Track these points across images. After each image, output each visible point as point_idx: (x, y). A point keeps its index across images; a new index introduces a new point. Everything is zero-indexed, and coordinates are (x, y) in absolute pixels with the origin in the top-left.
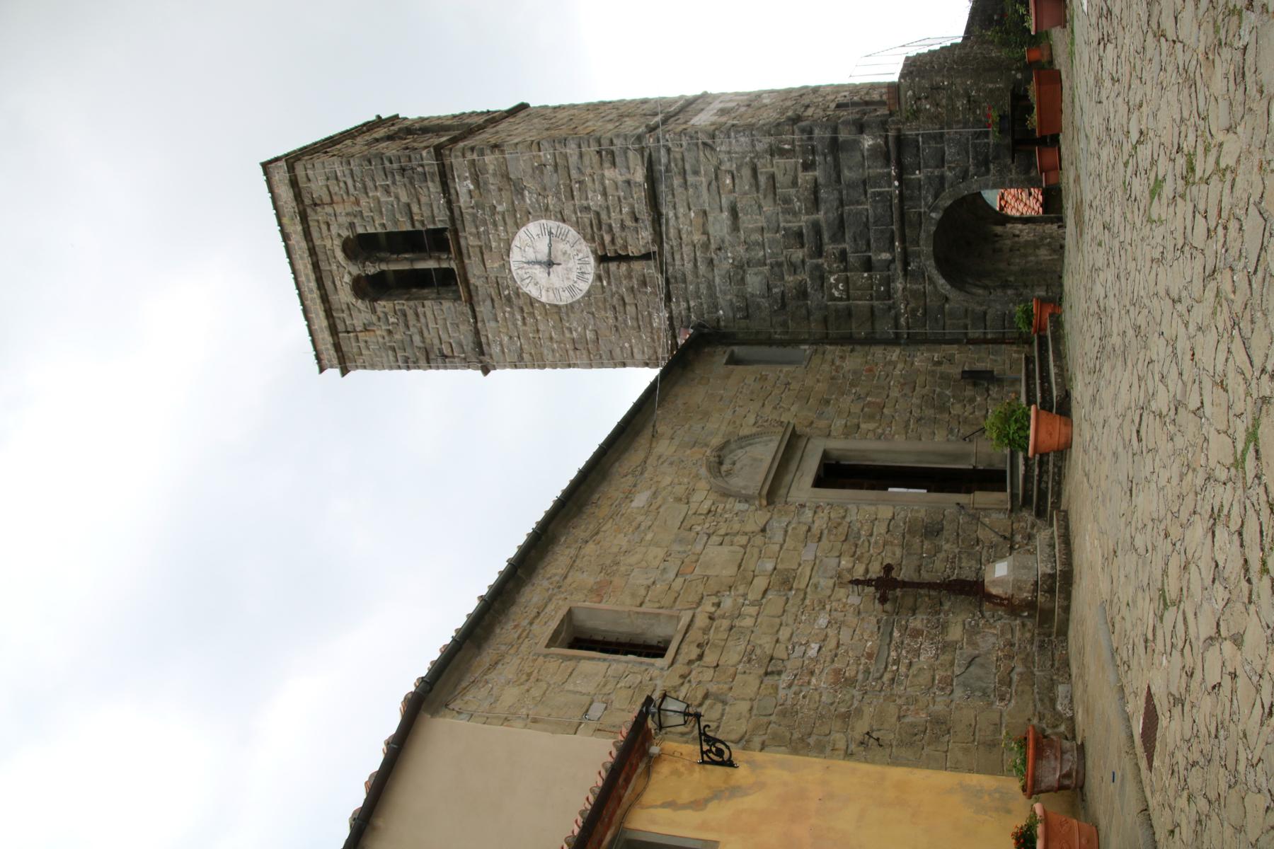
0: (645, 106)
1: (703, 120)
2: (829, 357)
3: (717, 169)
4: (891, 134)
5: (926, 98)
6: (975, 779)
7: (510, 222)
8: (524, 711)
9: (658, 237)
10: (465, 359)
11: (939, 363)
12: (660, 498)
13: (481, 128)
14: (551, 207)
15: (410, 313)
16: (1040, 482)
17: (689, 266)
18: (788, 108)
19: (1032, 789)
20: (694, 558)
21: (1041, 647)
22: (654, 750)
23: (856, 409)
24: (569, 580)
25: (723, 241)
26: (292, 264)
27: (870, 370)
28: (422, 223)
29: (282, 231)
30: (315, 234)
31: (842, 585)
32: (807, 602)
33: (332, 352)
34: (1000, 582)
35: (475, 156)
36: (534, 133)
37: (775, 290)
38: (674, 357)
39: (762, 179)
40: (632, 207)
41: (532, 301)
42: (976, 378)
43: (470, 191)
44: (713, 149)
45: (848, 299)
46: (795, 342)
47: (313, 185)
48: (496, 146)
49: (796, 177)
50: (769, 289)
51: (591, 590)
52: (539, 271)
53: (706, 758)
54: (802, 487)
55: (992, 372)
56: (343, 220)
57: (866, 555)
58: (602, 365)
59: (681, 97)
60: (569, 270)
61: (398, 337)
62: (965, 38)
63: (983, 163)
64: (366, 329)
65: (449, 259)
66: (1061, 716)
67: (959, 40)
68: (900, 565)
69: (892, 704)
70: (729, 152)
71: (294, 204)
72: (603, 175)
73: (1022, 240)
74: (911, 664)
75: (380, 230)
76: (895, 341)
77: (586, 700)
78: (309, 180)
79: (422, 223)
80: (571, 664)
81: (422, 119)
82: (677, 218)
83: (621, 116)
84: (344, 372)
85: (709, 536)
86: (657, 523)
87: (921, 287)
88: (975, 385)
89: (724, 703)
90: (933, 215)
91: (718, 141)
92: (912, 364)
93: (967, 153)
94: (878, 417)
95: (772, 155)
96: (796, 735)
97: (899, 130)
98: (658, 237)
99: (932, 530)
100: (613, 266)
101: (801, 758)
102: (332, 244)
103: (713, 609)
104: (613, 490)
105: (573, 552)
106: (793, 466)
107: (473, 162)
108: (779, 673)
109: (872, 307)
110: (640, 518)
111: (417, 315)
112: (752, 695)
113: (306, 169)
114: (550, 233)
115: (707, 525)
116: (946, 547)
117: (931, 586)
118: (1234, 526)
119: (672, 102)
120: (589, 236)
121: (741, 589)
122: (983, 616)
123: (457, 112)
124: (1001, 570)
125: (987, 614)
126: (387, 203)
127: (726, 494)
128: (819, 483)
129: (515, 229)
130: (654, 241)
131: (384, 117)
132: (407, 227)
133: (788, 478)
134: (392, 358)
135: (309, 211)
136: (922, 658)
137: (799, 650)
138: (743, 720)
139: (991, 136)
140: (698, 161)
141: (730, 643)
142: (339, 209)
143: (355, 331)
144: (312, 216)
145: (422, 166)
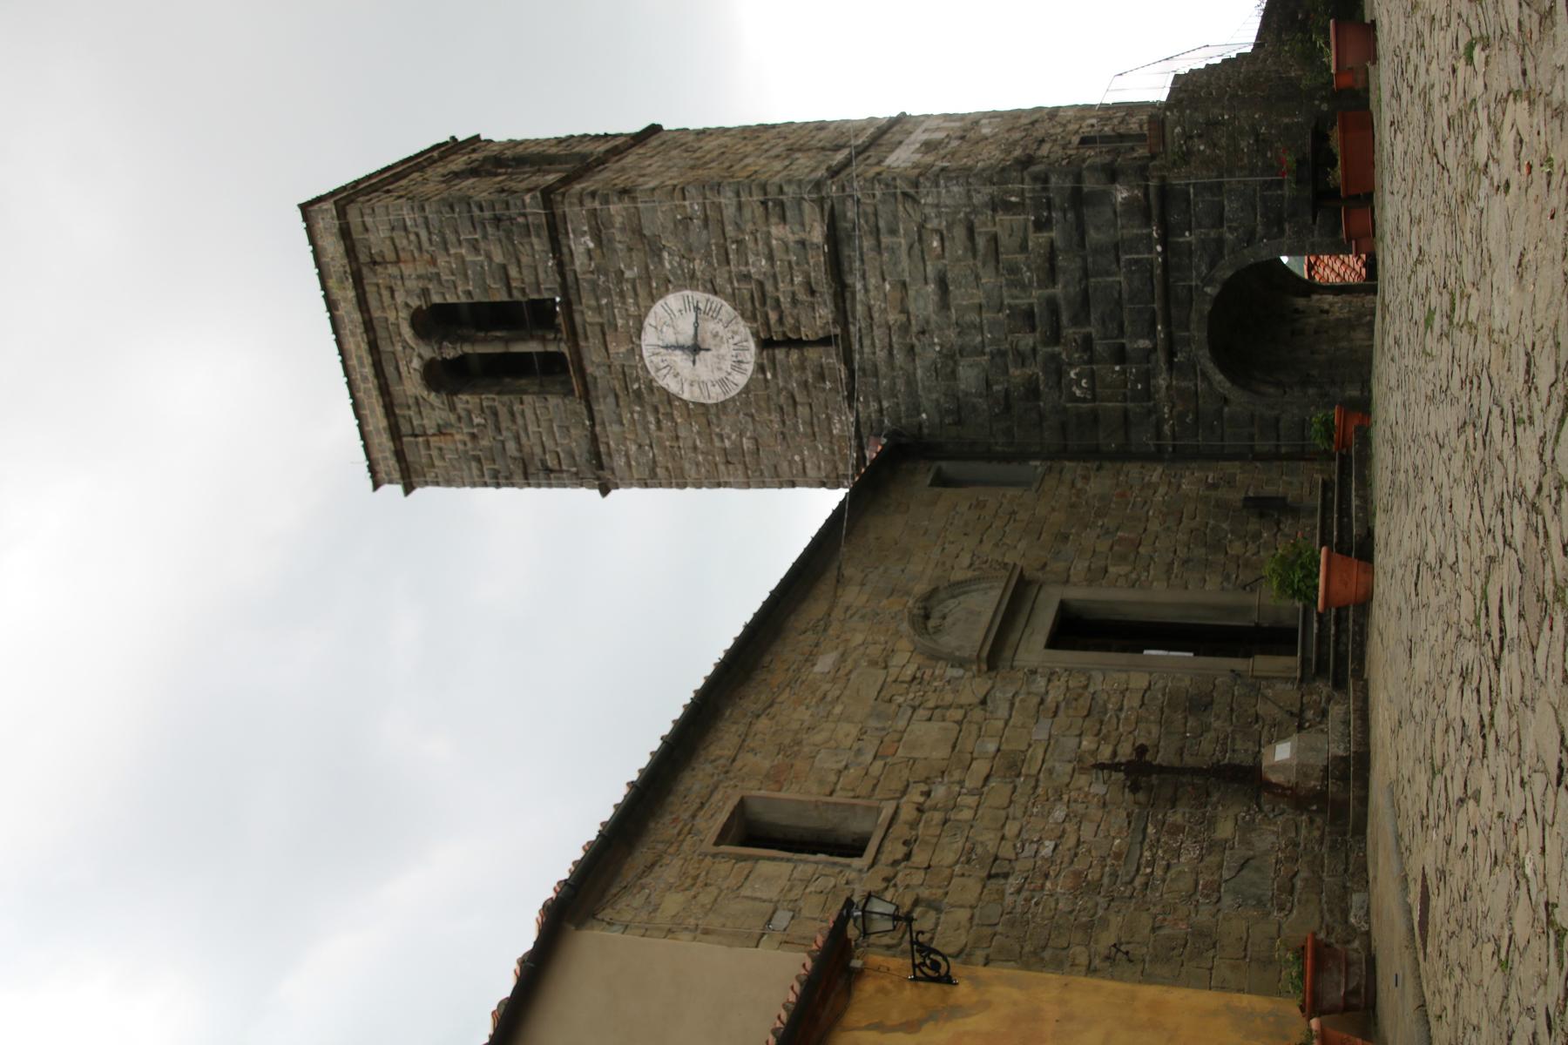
0: (822, 135)
1: (902, 158)
2: (1067, 477)
3: (921, 227)
4: (1153, 183)
5: (1200, 136)
6: (1245, 1000)
7: (642, 292)
8: (692, 921)
9: (843, 315)
10: (576, 474)
11: (1214, 486)
12: (850, 661)
13: (602, 161)
14: (699, 274)
15: (503, 413)
16: (1337, 642)
17: (881, 354)
18: (1015, 143)
19: (1313, 1007)
20: (896, 736)
21: (1332, 848)
22: (856, 963)
23: (1103, 546)
24: (738, 764)
25: (928, 322)
26: (339, 342)
27: (1123, 495)
28: (523, 291)
29: (327, 297)
30: (373, 302)
31: (1083, 770)
32: (1040, 791)
33: (392, 462)
34: (1282, 767)
35: (597, 204)
36: (674, 172)
37: (996, 388)
38: (862, 477)
39: (981, 242)
40: (807, 276)
41: (670, 398)
42: (1266, 508)
43: (589, 251)
44: (915, 201)
45: (1094, 399)
46: (1023, 456)
47: (372, 237)
48: (625, 192)
49: (1025, 240)
50: (988, 385)
51: (767, 776)
52: (680, 360)
53: (919, 974)
54: (1032, 648)
55: (1284, 499)
56: (412, 284)
57: (1114, 734)
58: (763, 485)
59: (872, 120)
60: (720, 358)
61: (484, 443)
62: (1257, 46)
63: (1276, 223)
64: (441, 431)
65: (557, 340)
66: (1354, 929)
67: (1249, 49)
68: (1157, 746)
69: (1145, 914)
70: (937, 206)
71: (345, 261)
72: (769, 233)
73: (1332, 317)
74: (1168, 866)
75: (464, 299)
76: (1157, 456)
77: (769, 907)
78: (366, 230)
79: (523, 291)
80: (747, 865)
81: (513, 144)
82: (867, 290)
83: (791, 150)
84: (408, 489)
85: (914, 709)
86: (847, 692)
87: (1191, 385)
88: (1262, 515)
89: (939, 910)
90: (1208, 290)
91: (923, 190)
92: (1179, 486)
93: (1254, 208)
94: (1132, 557)
95: (994, 210)
96: (1028, 948)
97: (1163, 179)
98: (843, 315)
99: (1199, 704)
100: (780, 354)
101: (1033, 974)
102: (397, 317)
103: (921, 799)
104: (788, 652)
105: (742, 729)
106: (1022, 620)
107: (593, 213)
108: (1006, 876)
109: (1126, 412)
110: (826, 687)
111: (512, 414)
112: (973, 902)
113: (362, 216)
114: (697, 309)
115: (911, 696)
116: (1217, 724)
117: (1195, 771)
118: (1474, 685)
119: (858, 127)
120: (749, 314)
121: (957, 775)
122: (1261, 810)
123: (563, 135)
124: (1283, 752)
125: (1267, 808)
126: (474, 263)
127: (935, 657)
128: (1054, 642)
129: (648, 303)
130: (835, 322)
131: (461, 138)
132: (502, 296)
133: (1014, 637)
134: (475, 472)
135: (365, 271)
136: (1182, 859)
137: (1030, 849)
138: (962, 931)
139: (1286, 187)
140: (895, 216)
141: (944, 840)
142: (407, 269)
143: (425, 434)
144: (369, 278)
145: (525, 215)
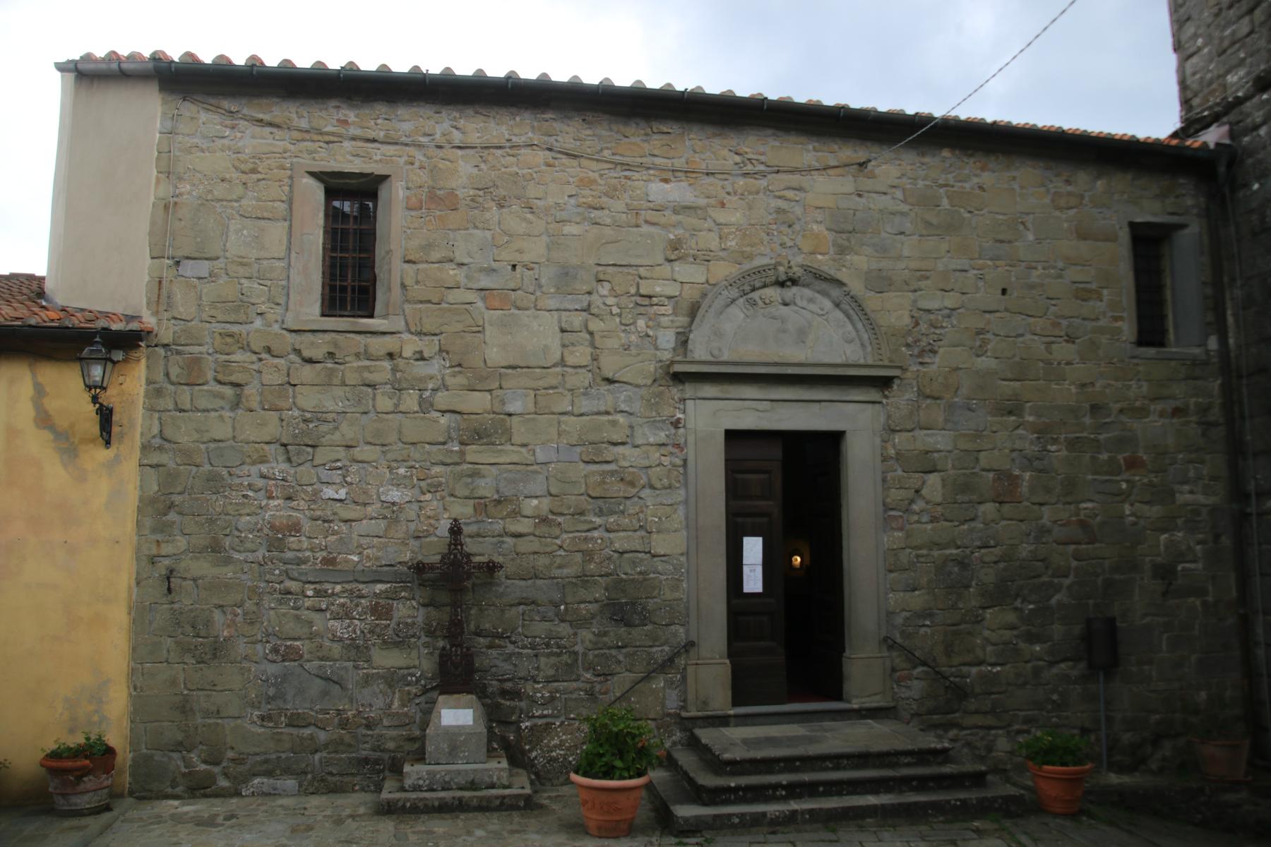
76: (1238, 492)
96: (177, 499)
112: (240, 438)
136: (336, 624)
138: (196, 436)
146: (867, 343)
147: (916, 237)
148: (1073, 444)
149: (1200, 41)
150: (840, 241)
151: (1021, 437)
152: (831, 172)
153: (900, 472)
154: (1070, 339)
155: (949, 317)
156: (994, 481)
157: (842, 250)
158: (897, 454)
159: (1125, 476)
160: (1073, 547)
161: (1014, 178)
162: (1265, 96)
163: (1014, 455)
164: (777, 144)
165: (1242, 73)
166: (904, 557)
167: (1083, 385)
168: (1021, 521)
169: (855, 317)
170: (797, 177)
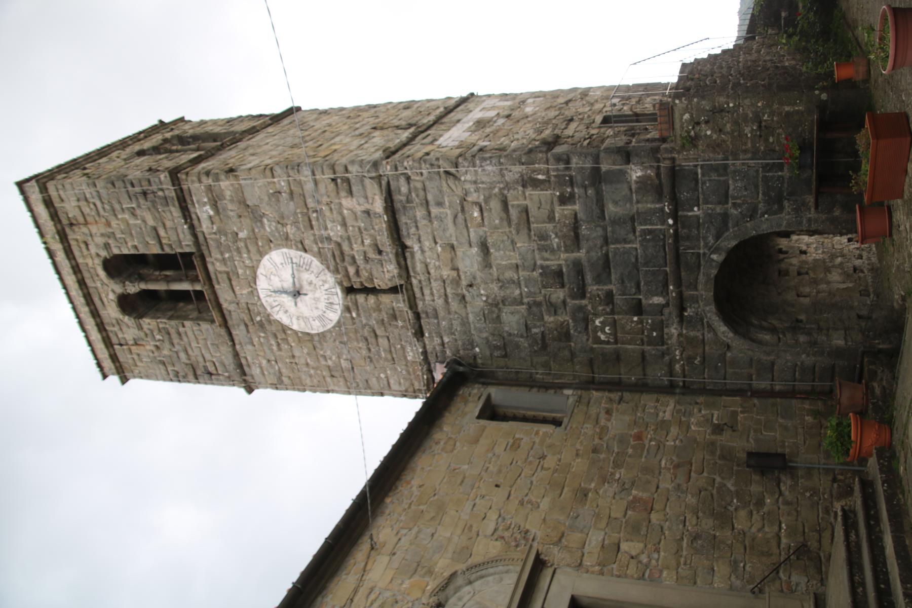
76: (669, 389)
95: (524, 186)
146: (506, 568)
147: (439, 527)
148: (617, 465)
149: (382, 376)
150: (422, 573)
151: (605, 492)
152: (368, 568)
153: (615, 566)
154: (543, 457)
155: (504, 519)
156: (634, 511)
157: (430, 572)
158: (599, 565)
159: (646, 442)
160: (692, 474)
161: (423, 469)
162: (427, 335)
163: (617, 497)
164: (330, 596)
165: (409, 349)
166: (684, 571)
167: (577, 455)
168: (668, 500)
169: (484, 572)
170: (361, 590)
